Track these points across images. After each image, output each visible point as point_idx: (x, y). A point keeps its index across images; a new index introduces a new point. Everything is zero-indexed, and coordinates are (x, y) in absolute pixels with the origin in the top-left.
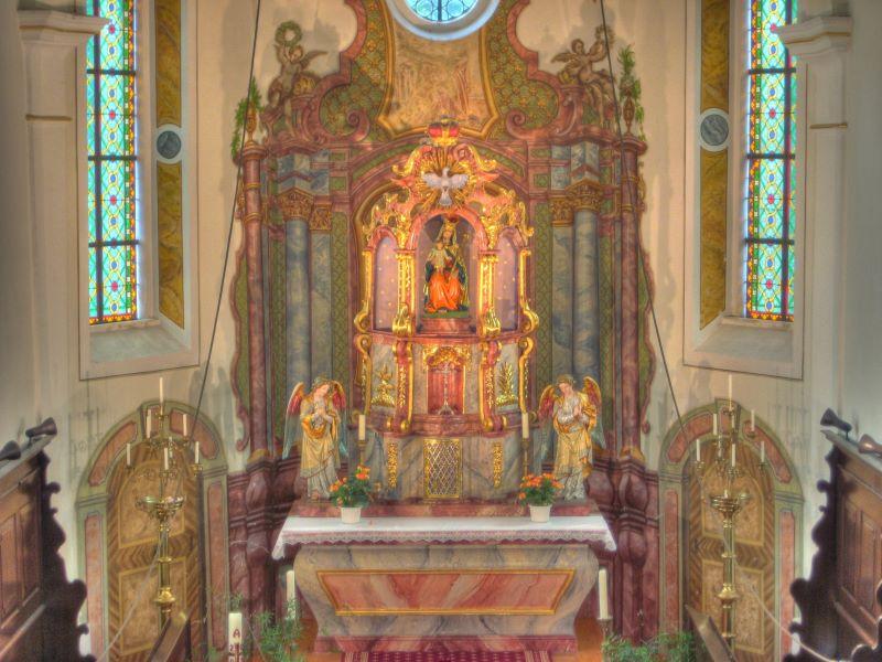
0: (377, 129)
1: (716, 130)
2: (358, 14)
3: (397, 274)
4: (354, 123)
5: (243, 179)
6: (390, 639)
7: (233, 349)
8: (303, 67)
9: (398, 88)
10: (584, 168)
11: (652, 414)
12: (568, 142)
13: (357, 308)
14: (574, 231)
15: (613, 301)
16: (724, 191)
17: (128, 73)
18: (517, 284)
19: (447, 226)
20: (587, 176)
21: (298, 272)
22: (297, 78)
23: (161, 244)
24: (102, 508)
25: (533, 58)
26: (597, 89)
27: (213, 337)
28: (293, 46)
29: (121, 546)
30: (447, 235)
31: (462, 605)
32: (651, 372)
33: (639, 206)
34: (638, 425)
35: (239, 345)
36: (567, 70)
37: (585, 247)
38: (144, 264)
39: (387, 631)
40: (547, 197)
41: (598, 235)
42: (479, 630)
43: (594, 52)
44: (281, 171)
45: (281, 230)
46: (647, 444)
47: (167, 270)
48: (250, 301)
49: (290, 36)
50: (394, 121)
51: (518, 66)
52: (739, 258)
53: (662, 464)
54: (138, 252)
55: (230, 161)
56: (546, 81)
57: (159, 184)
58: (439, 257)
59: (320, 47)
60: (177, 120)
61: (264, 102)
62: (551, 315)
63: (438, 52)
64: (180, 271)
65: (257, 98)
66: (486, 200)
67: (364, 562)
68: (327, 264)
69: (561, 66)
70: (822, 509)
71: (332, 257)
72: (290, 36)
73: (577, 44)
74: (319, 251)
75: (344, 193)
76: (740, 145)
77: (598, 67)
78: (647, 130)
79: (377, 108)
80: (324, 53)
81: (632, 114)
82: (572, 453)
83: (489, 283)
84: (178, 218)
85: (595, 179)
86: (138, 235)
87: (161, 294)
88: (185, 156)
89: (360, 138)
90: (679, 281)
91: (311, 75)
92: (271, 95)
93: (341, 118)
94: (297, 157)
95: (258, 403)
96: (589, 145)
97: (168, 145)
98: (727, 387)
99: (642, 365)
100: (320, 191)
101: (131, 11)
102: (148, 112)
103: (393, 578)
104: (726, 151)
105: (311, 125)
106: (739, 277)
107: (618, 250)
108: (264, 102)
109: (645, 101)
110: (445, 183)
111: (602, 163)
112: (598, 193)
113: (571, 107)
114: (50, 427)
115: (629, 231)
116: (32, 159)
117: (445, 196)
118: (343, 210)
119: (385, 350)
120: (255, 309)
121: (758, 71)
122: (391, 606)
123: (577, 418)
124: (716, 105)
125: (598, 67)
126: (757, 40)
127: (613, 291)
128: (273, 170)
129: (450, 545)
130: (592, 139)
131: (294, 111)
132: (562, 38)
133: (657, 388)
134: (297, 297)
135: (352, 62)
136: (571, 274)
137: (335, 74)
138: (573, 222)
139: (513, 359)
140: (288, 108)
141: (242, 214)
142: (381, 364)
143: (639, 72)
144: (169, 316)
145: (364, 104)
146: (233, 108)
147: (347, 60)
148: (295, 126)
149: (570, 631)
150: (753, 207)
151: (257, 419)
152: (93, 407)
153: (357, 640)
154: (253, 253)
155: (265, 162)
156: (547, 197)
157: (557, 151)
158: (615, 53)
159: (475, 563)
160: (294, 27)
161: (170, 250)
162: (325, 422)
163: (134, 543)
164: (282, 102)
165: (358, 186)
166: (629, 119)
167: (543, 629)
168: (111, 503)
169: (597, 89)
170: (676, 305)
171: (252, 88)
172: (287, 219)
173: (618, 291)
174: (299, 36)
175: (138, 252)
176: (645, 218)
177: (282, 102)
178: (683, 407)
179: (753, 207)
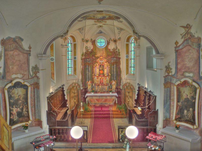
0: (95, 56)
1: (127, 56)
3: (97, 71)
4: (93, 56)
5: (82, 61)
6: (96, 105)
11: (121, 84)
12: (113, 58)
13: (93, 74)
19: (102, 66)
24: (69, 93)
25: (110, 50)
31: (103, 102)
32: (121, 79)
33: (120, 64)
37: (115, 68)
39: (96, 104)
40: (111, 63)
41: (116, 67)
42: (105, 104)
44: (86, 61)
45: (86, 66)
47: (75, 70)
49: (87, 48)
50: (97, 56)
53: (122, 88)
56: (111, 52)
58: (101, 69)
61: (84, 54)
62: (112, 74)
66: (105, 63)
67: (94, 98)
69: (113, 50)
73: (114, 48)
77: (116, 51)
79: (95, 55)
81: (119, 55)
83: (106, 71)
85: (116, 61)
88: (77, 59)
93: (91, 56)
97: (75, 58)
98: (129, 81)
102: (73, 55)
103: (97, 99)
105: (89, 56)
108: (84, 54)
113: (113, 54)
119: (96, 78)
122: (97, 102)
125: (116, 51)
126: (131, 48)
129: (102, 96)
130: (116, 57)
132: (113, 48)
133: (122, 81)
134: (87, 72)
138: (114, 65)
140: (86, 55)
147: (92, 50)
149: (113, 104)
151: (84, 84)
153: (93, 105)
156: (111, 63)
157: (112, 59)
158: (118, 49)
159: (104, 98)
160: (87, 47)
164: (86, 54)
167: (111, 104)
171: (83, 53)
174: (87, 48)
177: (86, 54)
178: (124, 83)
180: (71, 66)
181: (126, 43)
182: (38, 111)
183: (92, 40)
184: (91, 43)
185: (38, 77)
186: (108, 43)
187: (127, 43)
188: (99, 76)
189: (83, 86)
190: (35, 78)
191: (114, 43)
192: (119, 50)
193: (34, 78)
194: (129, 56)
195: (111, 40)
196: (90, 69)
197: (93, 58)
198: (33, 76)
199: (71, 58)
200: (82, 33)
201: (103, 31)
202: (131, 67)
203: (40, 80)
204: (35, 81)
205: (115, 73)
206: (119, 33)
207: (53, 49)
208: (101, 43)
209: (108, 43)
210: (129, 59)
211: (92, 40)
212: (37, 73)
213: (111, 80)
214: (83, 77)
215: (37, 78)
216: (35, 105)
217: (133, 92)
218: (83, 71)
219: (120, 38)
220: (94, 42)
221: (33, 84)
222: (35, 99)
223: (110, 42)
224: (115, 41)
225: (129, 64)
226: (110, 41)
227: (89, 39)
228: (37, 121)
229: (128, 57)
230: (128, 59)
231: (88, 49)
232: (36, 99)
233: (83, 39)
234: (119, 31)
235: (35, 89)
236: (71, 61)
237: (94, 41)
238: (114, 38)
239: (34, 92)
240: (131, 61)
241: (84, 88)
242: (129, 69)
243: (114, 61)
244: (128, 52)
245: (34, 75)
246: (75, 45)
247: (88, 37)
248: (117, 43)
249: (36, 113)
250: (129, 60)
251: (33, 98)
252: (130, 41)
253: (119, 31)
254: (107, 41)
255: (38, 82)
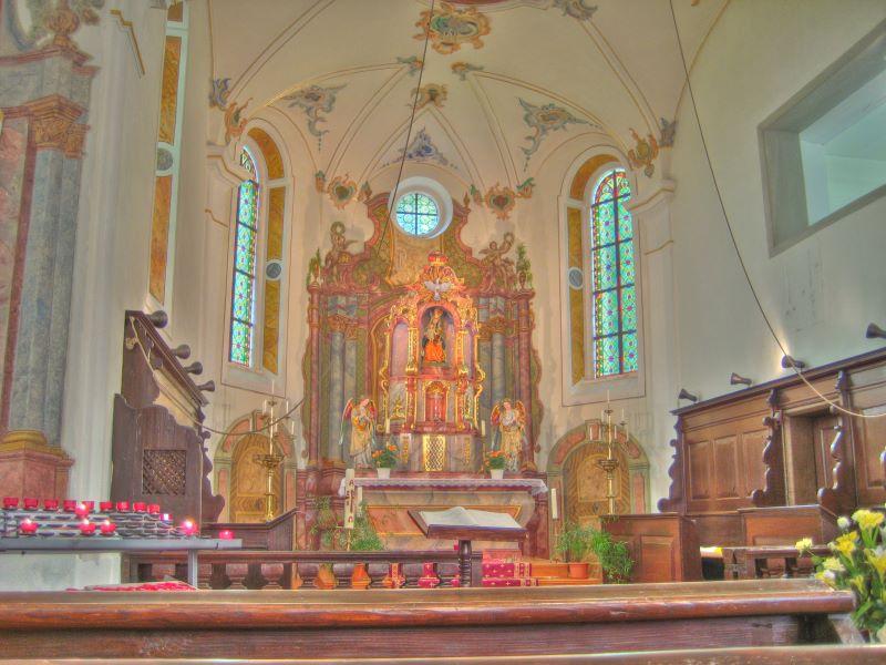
0: (384, 284)
1: (577, 278)
2: (375, 224)
3: (406, 342)
4: (372, 281)
5: (311, 301)
7: (303, 396)
8: (344, 248)
9: (396, 260)
10: (497, 310)
12: (488, 296)
13: (380, 364)
14: (492, 345)
15: (514, 382)
16: (582, 312)
17: (253, 229)
18: (473, 354)
19: (437, 313)
20: (498, 314)
21: (337, 360)
22: (341, 254)
23: (266, 327)
24: (228, 467)
25: (469, 251)
26: (503, 269)
27: (295, 389)
28: (340, 236)
29: (238, 495)
30: (435, 321)
32: (541, 415)
33: (530, 326)
34: (532, 449)
35: (306, 394)
36: (487, 258)
37: (497, 353)
38: (255, 338)
41: (504, 347)
43: (501, 248)
44: (330, 304)
45: (330, 337)
46: (538, 459)
47: (269, 341)
48: (312, 371)
49: (339, 230)
50: (394, 280)
51: (461, 255)
52: (591, 349)
53: (548, 466)
54: (251, 330)
55: (305, 289)
56: (476, 264)
57: (267, 294)
58: (431, 333)
59: (355, 239)
60: (279, 257)
61: (323, 264)
63: (418, 244)
64: (277, 342)
65: (319, 260)
66: (459, 299)
68: (354, 358)
69: (484, 256)
70: (674, 456)
71: (357, 354)
72: (339, 230)
73: (493, 244)
74: (350, 349)
75: (365, 319)
76: (589, 284)
77: (503, 257)
78: (535, 285)
79: (385, 273)
80: (356, 242)
81: (524, 278)
82: (511, 444)
83: (461, 345)
84: (277, 311)
86: (252, 321)
87: (264, 356)
88: (283, 276)
89: (374, 288)
90: (559, 363)
91: (349, 254)
92: (327, 261)
93: (364, 277)
94: (340, 297)
95: (313, 432)
96: (499, 298)
97: (273, 271)
98: (588, 414)
99: (534, 413)
100: (351, 316)
101: (256, 197)
102: (262, 251)
104: (582, 290)
105: (347, 280)
106: (592, 357)
107: (517, 353)
108: (323, 264)
109: (532, 270)
110: (438, 287)
111: (506, 308)
112: (505, 324)
113: (489, 278)
114: (210, 386)
115: (524, 341)
116: (107, 589)
117: (437, 294)
118: (365, 327)
119: (399, 387)
120: (314, 377)
121: (598, 248)
123: (514, 422)
124: (575, 264)
125: (503, 257)
126: (596, 231)
127: (514, 376)
128: (326, 303)
131: (339, 273)
132: (485, 242)
134: (337, 375)
135: (371, 248)
136: (18, 345)
137: (361, 254)
139: (471, 396)
140: (335, 269)
141: (310, 321)
142: (395, 395)
143: (527, 256)
144: (269, 369)
145: (377, 269)
146: (308, 262)
147: (368, 246)
148: (339, 280)
150: (598, 319)
151: (313, 440)
152: (228, 403)
154: (314, 344)
155: (322, 296)
157: (482, 301)
158: (514, 247)
160: (342, 226)
161: (271, 329)
162: (367, 422)
163: (245, 496)
164: (332, 266)
165: (373, 315)
166: (522, 282)
168: (234, 464)
169: (503, 269)
170: (556, 375)
171: (318, 255)
172: (332, 331)
173: (517, 376)
174: (343, 231)
175: (251, 330)
176: (534, 332)
177: (332, 266)
178: (561, 432)
179: (598, 319)
180: (248, 313)
181: (566, 201)
182: (44, 358)
183: (367, 190)
184: (364, 209)
185: (80, 62)
186: (461, 215)
187: (575, 204)
188: (421, 368)
189: (309, 453)
190: (56, 66)
191: (495, 216)
192: (521, 252)
193: (48, 62)
194: (585, 274)
195: (478, 200)
196: (351, 354)
197: (372, 294)
198: (39, 43)
199: (251, 268)
200: (320, 134)
201: (439, 140)
202: (598, 337)
203: (95, 81)
204: (50, 90)
205: (498, 385)
206: (526, 152)
207: (175, 93)
208: (419, 218)
209: (461, 215)
210: (587, 296)
211: (367, 190)
212: (77, 24)
213: (487, 402)
214: (314, 396)
215: (67, 64)
216: (16, 295)
217: (631, 472)
218: (314, 358)
219: (528, 181)
220: (380, 207)
221: (22, 111)
222: (29, 244)
223: (468, 211)
224: (501, 202)
225: (586, 323)
226: (472, 205)
227: (357, 181)
228: (14, 457)
229: (581, 281)
230: (582, 290)
231: (348, 236)
232: (36, 238)
233: (320, 178)
234: (529, 138)
235: (45, 157)
236: (249, 286)
237: (379, 196)
238: (493, 184)
239: (29, 179)
240: (600, 301)
241: (315, 469)
242: (587, 349)
243: (491, 317)
244: (578, 255)
245: (50, 36)
246: (276, 197)
247: (354, 171)
248: (514, 214)
249: (25, 372)
250: (587, 303)
251: (14, 231)
252: (590, 195)
253: (529, 138)
254: (455, 203)
255: (76, 100)
